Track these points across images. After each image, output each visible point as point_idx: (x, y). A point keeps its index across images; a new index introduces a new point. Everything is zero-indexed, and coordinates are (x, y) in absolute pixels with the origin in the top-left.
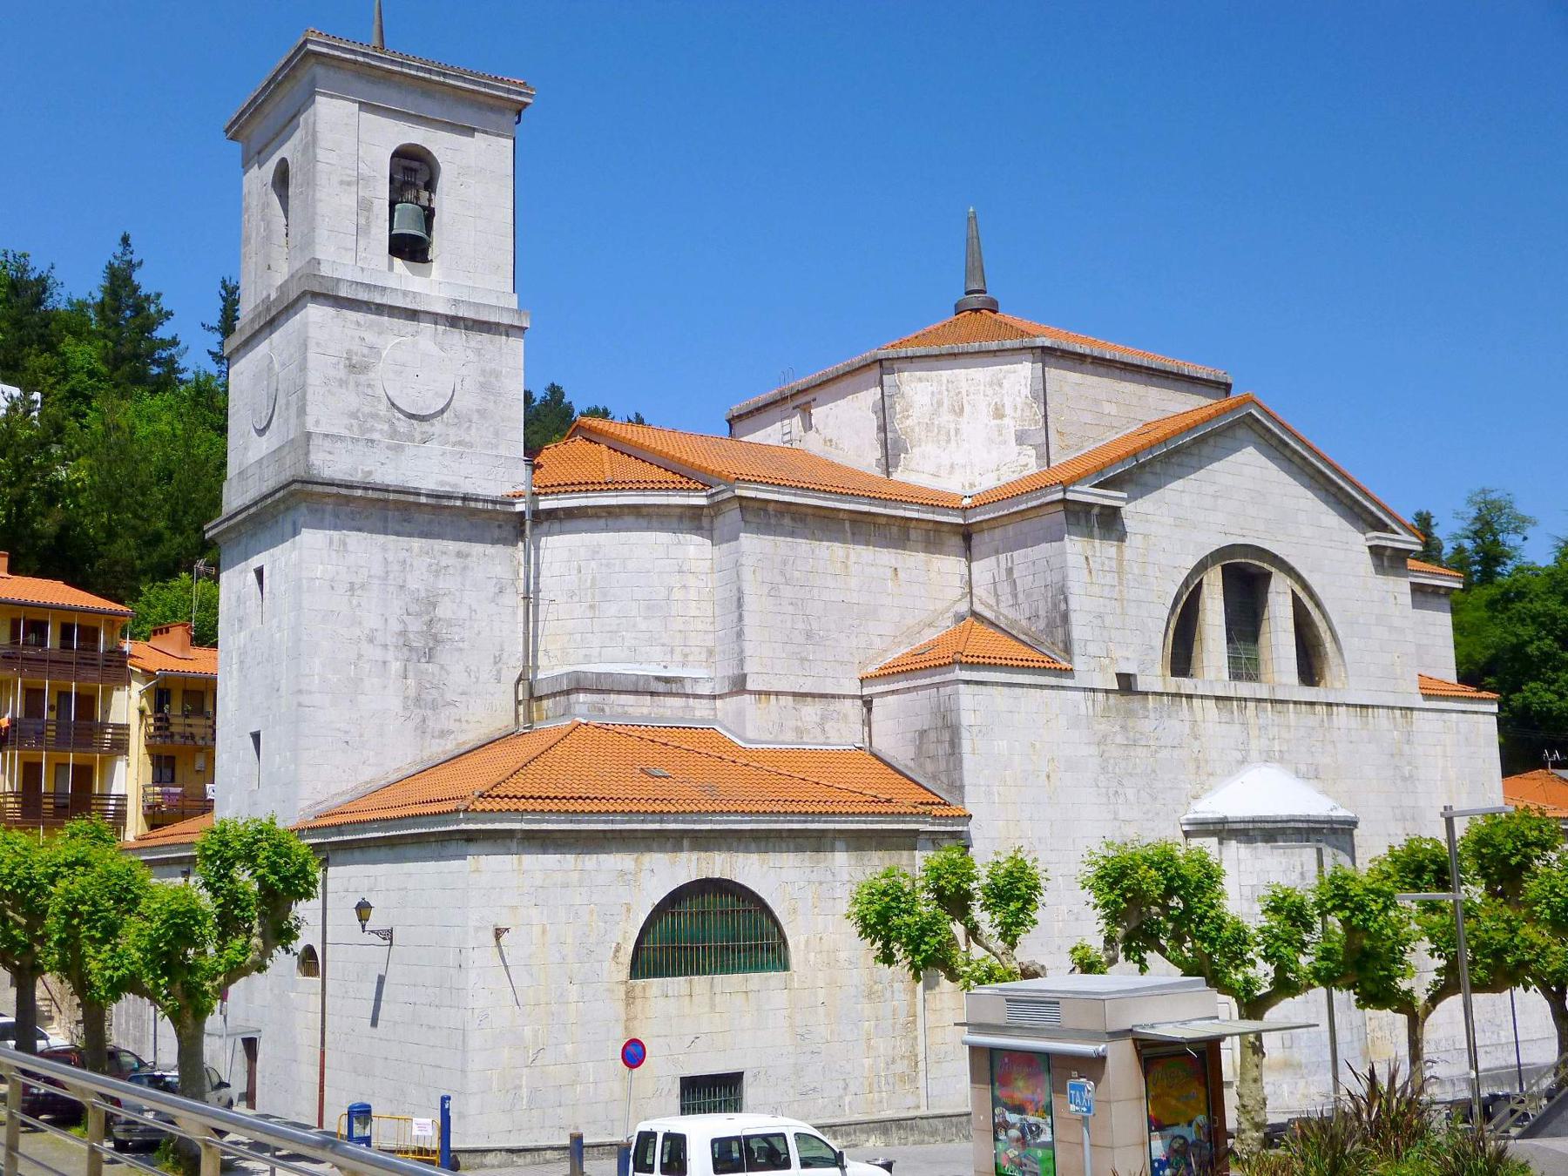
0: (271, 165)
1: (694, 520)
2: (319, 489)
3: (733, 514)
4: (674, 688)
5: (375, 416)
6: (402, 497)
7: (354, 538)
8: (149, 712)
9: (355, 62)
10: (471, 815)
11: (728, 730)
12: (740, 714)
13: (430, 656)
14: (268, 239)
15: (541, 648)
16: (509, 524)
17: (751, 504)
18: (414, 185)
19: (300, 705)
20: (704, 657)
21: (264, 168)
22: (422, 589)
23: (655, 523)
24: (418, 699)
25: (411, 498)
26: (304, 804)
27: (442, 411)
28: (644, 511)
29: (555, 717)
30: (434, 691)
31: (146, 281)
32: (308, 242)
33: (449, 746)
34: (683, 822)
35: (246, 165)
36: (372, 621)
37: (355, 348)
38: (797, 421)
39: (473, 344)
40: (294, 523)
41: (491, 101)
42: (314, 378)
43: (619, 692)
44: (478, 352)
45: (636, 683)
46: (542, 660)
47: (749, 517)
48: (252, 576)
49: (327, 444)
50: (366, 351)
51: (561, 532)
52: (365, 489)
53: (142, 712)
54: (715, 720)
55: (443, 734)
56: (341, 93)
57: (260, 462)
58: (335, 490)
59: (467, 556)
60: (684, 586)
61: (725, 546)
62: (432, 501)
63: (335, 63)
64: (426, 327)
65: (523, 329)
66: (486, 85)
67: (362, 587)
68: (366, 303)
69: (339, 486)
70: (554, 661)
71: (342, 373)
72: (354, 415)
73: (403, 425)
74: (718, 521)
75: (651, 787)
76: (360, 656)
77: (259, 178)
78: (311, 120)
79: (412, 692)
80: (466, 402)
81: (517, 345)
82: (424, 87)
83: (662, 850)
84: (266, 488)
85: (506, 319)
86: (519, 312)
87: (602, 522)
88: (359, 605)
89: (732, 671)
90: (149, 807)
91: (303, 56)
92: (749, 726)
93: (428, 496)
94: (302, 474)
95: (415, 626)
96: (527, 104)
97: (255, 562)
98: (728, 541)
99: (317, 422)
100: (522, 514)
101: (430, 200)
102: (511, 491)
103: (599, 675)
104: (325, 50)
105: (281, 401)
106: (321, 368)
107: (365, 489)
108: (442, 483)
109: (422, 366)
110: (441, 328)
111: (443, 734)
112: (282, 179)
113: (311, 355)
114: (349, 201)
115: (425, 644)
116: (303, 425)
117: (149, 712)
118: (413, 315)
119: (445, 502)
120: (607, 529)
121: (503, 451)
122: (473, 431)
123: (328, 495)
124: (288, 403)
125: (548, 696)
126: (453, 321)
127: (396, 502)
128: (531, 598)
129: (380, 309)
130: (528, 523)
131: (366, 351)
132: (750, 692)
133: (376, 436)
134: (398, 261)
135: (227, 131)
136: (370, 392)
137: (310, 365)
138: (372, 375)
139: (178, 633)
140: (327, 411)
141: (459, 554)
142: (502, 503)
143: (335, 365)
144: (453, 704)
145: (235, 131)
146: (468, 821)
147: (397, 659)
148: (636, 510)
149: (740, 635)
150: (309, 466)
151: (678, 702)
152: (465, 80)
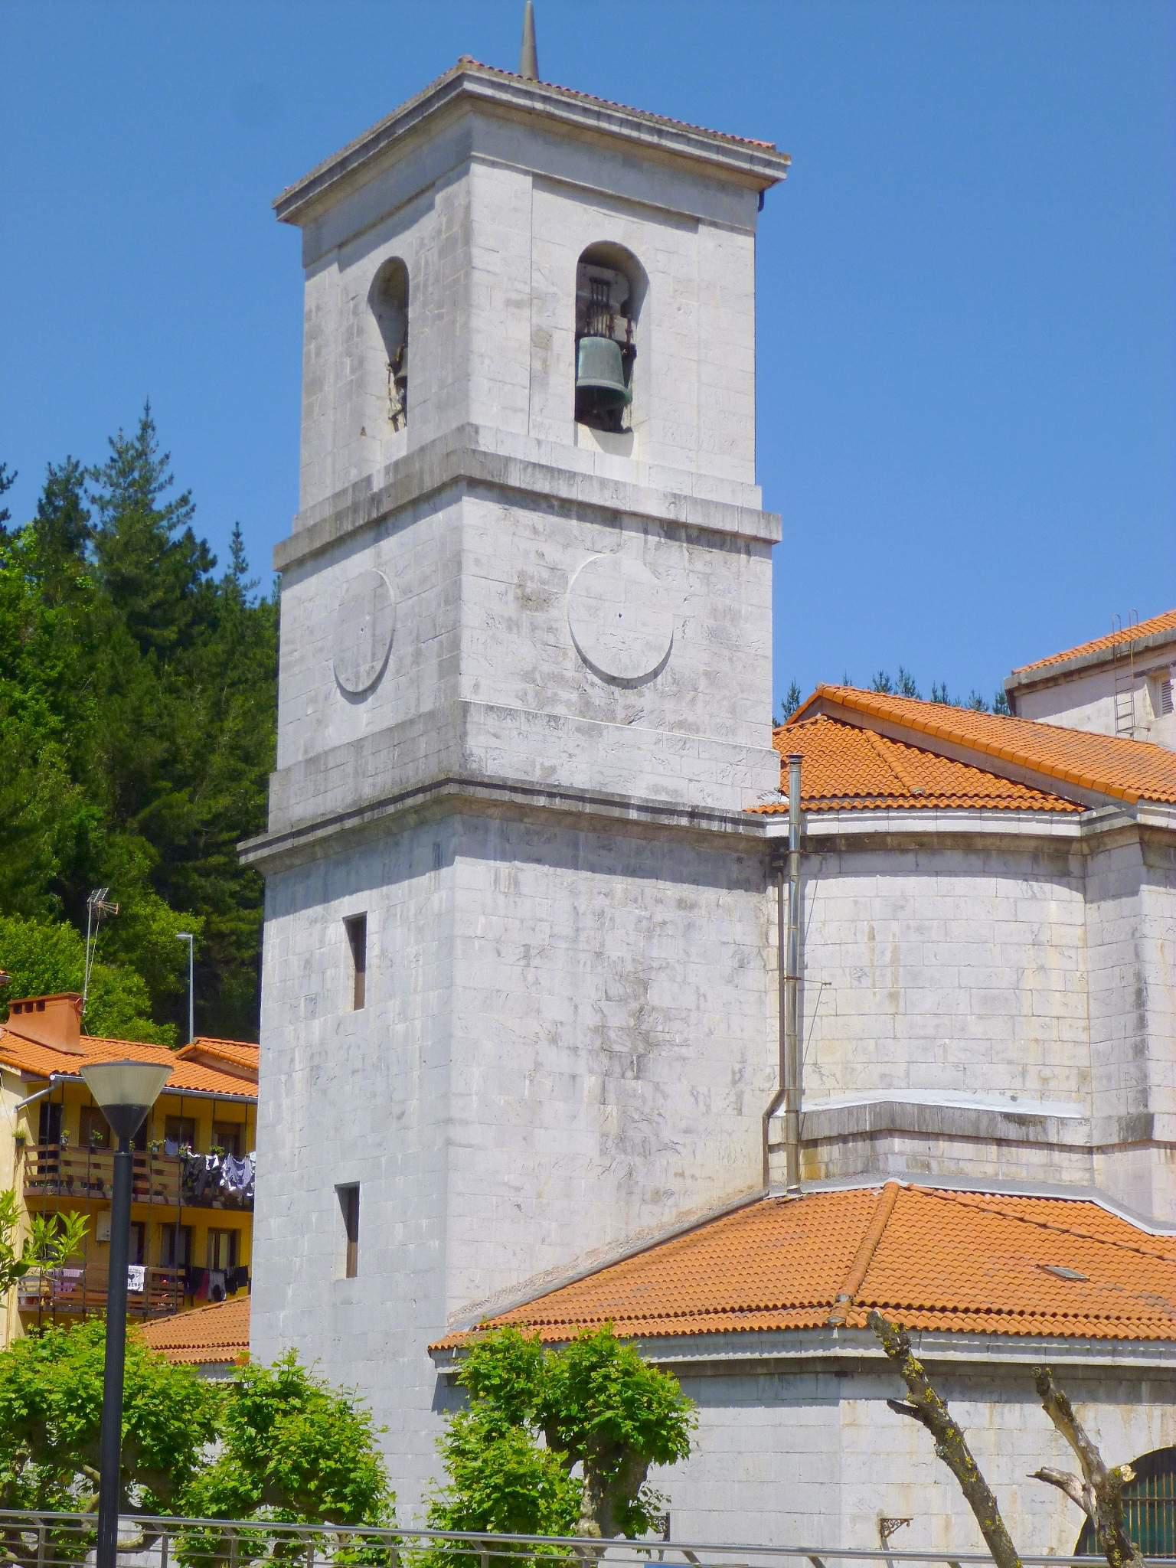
0: (370, 265)
1: (1055, 860)
2: (482, 793)
3: (1129, 854)
4: (1032, 1133)
5: (558, 679)
6: (604, 810)
7: (531, 874)
8: (30, 1142)
9: (531, 111)
10: (850, 1334)
11: (1120, 1206)
12: (1141, 1179)
13: (638, 1066)
14: (358, 386)
15: (808, 1060)
16: (765, 860)
17: (1157, 837)
18: (606, 307)
19: (449, 1142)
20: (1073, 1084)
21: (354, 270)
22: (628, 957)
23: (995, 863)
24: (622, 1139)
25: (616, 812)
26: (454, 1306)
27: (655, 673)
28: (979, 843)
29: (846, 1175)
30: (643, 1126)
31: (161, 443)
32: (457, 393)
33: (660, 1220)
34: (1144, 1355)
35: (313, 260)
36: (555, 1010)
37: (531, 569)
38: (1142, 696)
39: (699, 566)
40: (437, 846)
41: (723, 175)
42: (472, 616)
43: (952, 1137)
44: (706, 578)
45: (976, 1124)
46: (809, 1080)
47: (1153, 859)
48: (339, 933)
49: (491, 722)
50: (545, 574)
51: (841, 873)
52: (551, 795)
53: (20, 1141)
54: (1092, 1187)
55: (659, 1196)
56: (506, 160)
57: (358, 745)
58: (506, 796)
59: (692, 906)
60: (1042, 968)
61: (1108, 905)
62: (645, 817)
63: (500, 111)
64: (632, 537)
65: (769, 542)
66: (719, 150)
67: (541, 952)
68: (547, 497)
69: (514, 789)
70: (830, 1083)
71: (511, 609)
72: (528, 676)
73: (599, 693)
74: (1099, 862)
75: (1070, 1298)
76: (538, 1065)
77: (340, 291)
78: (461, 201)
79: (613, 1128)
80: (689, 660)
81: (761, 570)
82: (630, 153)
83: (1111, 1398)
84: (369, 791)
85: (749, 528)
86: (766, 514)
87: (910, 858)
88: (537, 982)
89: (1123, 1106)
90: (31, 1300)
91: (452, 96)
92: (1157, 1199)
93: (640, 808)
94: (455, 771)
95: (618, 1018)
96: (775, 180)
97: (349, 905)
98: (1116, 896)
99: (477, 686)
100: (783, 841)
101: (629, 332)
102: (756, 804)
103: (922, 1108)
104: (489, 92)
105: (404, 649)
106: (482, 599)
107: (551, 795)
108: (656, 789)
109: (629, 600)
110: (653, 539)
111: (659, 1196)
112: (392, 292)
113: (468, 581)
114: (520, 332)
115: (631, 1050)
116: (455, 689)
117: (30, 1142)
118: (612, 517)
119: (665, 820)
120: (917, 871)
121: (742, 740)
122: (700, 704)
123: (495, 803)
124: (418, 655)
125: (829, 1140)
126: (671, 529)
127: (593, 817)
128: (792, 980)
129: (567, 507)
130: (794, 857)
131: (545, 574)
132: (1160, 1145)
133: (560, 710)
134: (584, 429)
135: (279, 208)
136: (552, 640)
137: (466, 594)
138: (554, 613)
139: (60, 1010)
140: (489, 673)
141: (681, 904)
142: (747, 823)
143: (502, 595)
144: (672, 1147)
145: (295, 208)
146: (844, 1343)
147: (591, 1071)
148: (965, 841)
149: (1140, 1049)
150: (465, 757)
151: (1036, 1156)
152: (689, 141)
